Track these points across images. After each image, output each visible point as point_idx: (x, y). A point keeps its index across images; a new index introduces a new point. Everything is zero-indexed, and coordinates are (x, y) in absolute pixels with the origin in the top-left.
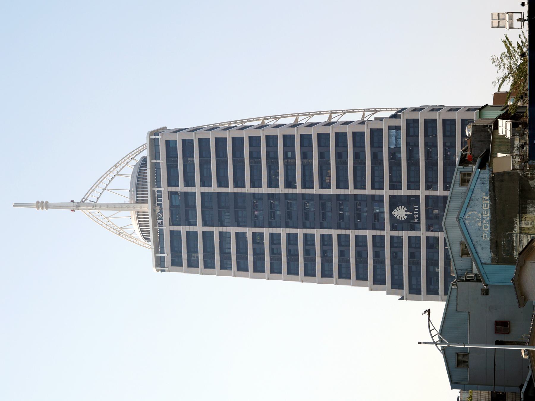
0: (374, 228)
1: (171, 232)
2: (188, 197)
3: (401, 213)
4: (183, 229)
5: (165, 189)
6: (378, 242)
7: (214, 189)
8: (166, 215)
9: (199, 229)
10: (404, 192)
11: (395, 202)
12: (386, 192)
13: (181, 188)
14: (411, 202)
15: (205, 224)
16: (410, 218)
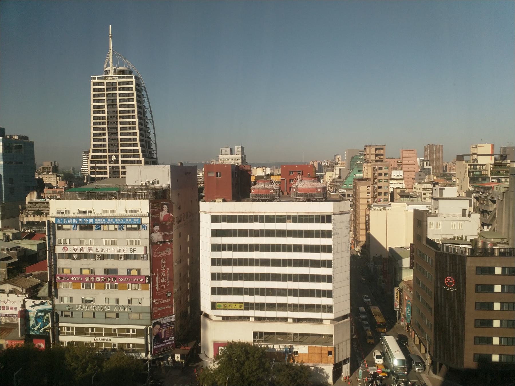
0: (109, 150)
1: (104, 83)
2: (114, 89)
3: (114, 158)
4: (105, 87)
5: (118, 81)
6: (105, 151)
7: (118, 98)
8: (109, 81)
9: (106, 92)
10: (120, 159)
11: (117, 156)
12: (120, 154)
13: (118, 87)
14: (117, 161)
15: (107, 94)
16: (112, 161)
